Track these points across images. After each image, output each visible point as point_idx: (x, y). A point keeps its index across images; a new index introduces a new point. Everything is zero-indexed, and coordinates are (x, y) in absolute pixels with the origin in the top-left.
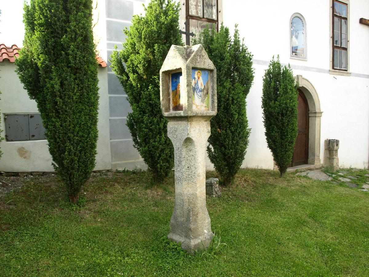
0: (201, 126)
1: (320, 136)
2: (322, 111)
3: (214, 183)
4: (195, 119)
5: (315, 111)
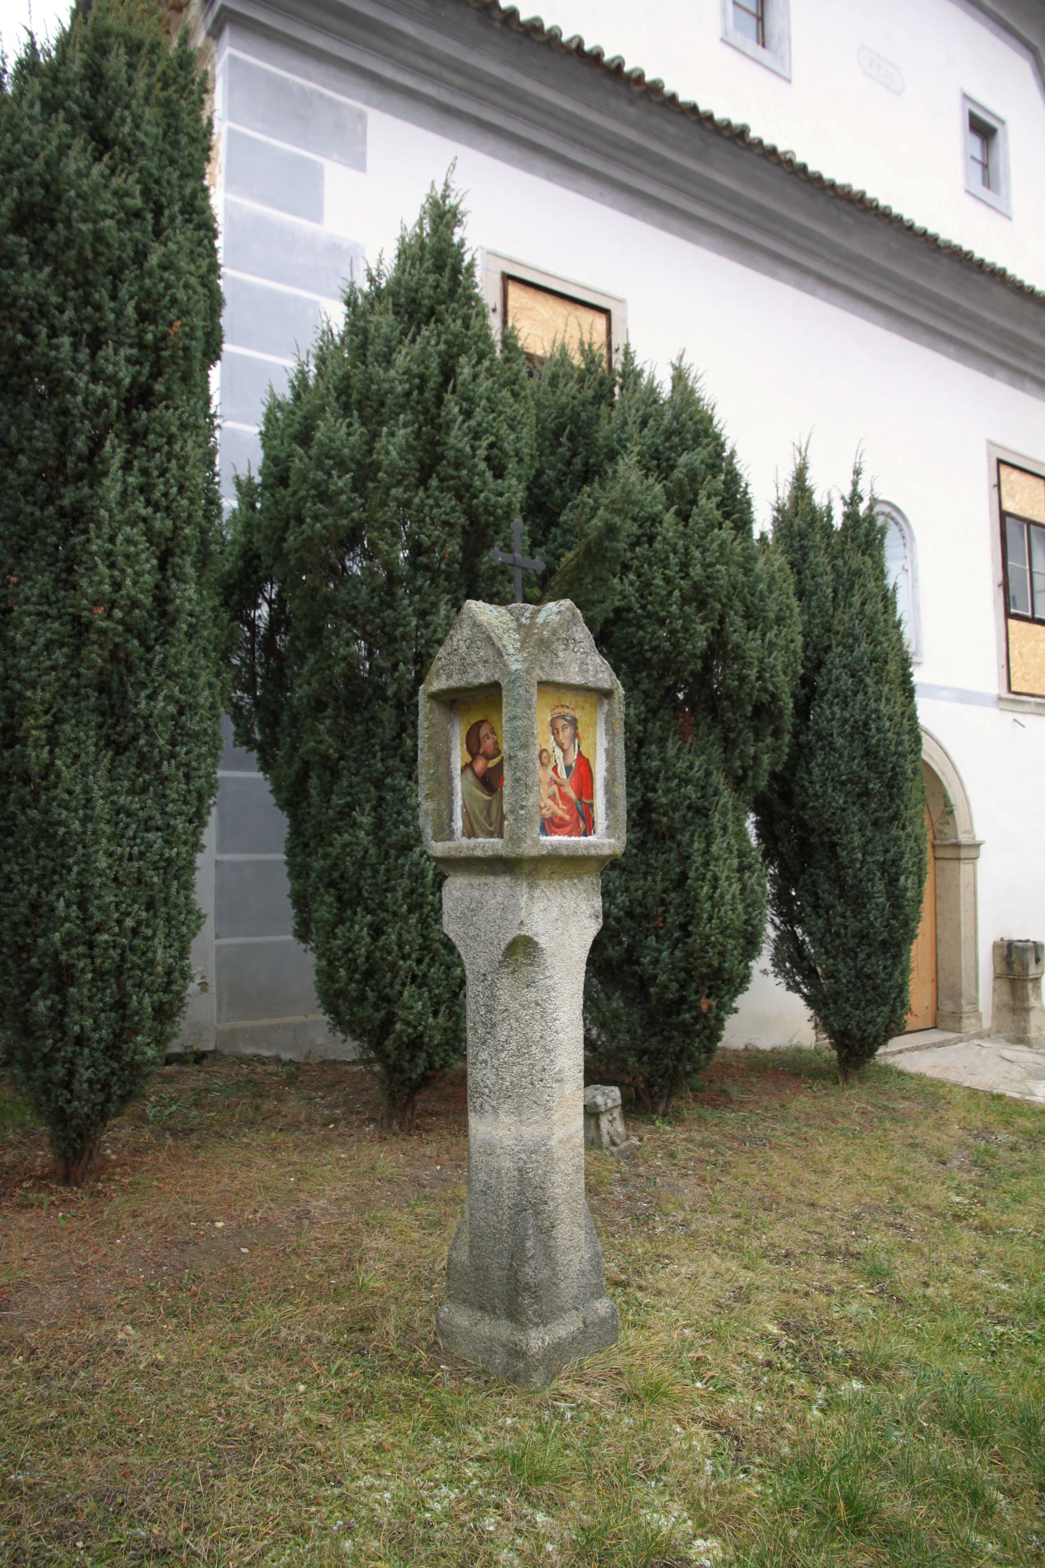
2: (979, 838)
5: (956, 837)
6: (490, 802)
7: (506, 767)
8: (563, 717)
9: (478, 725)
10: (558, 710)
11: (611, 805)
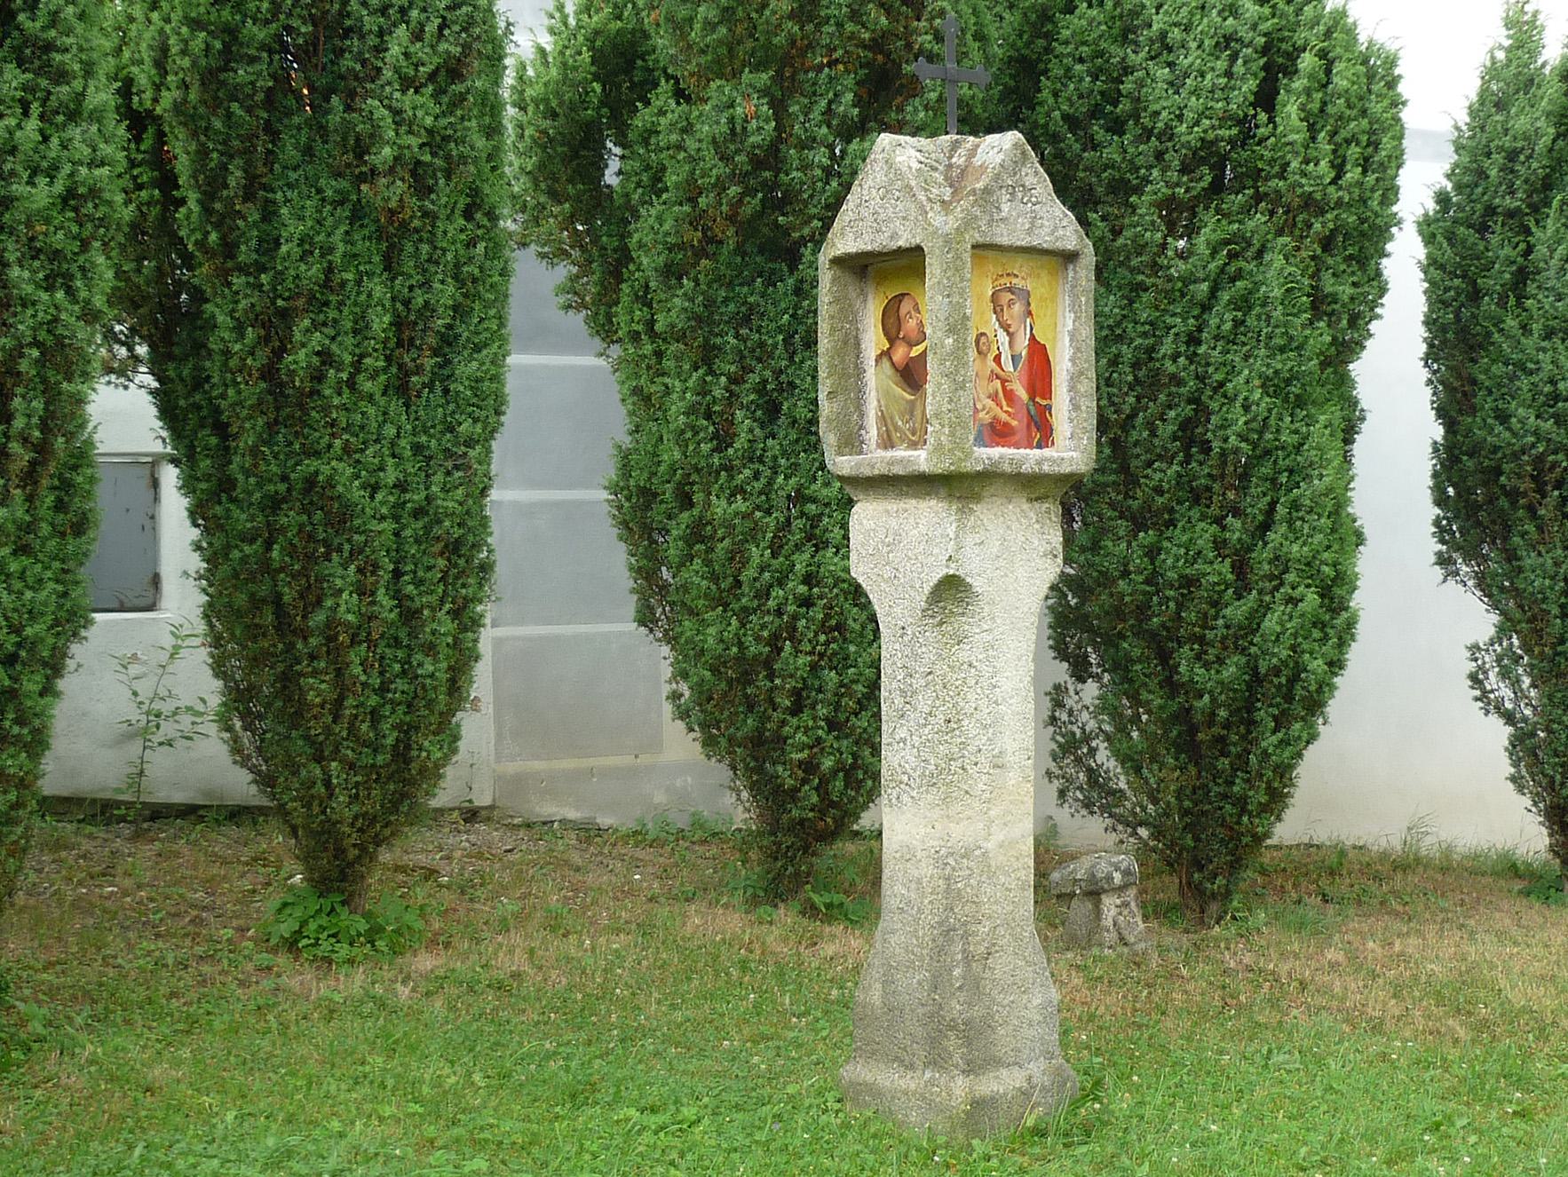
3: (1109, 878)
7: (929, 359)
8: (1010, 290)
10: (1002, 281)
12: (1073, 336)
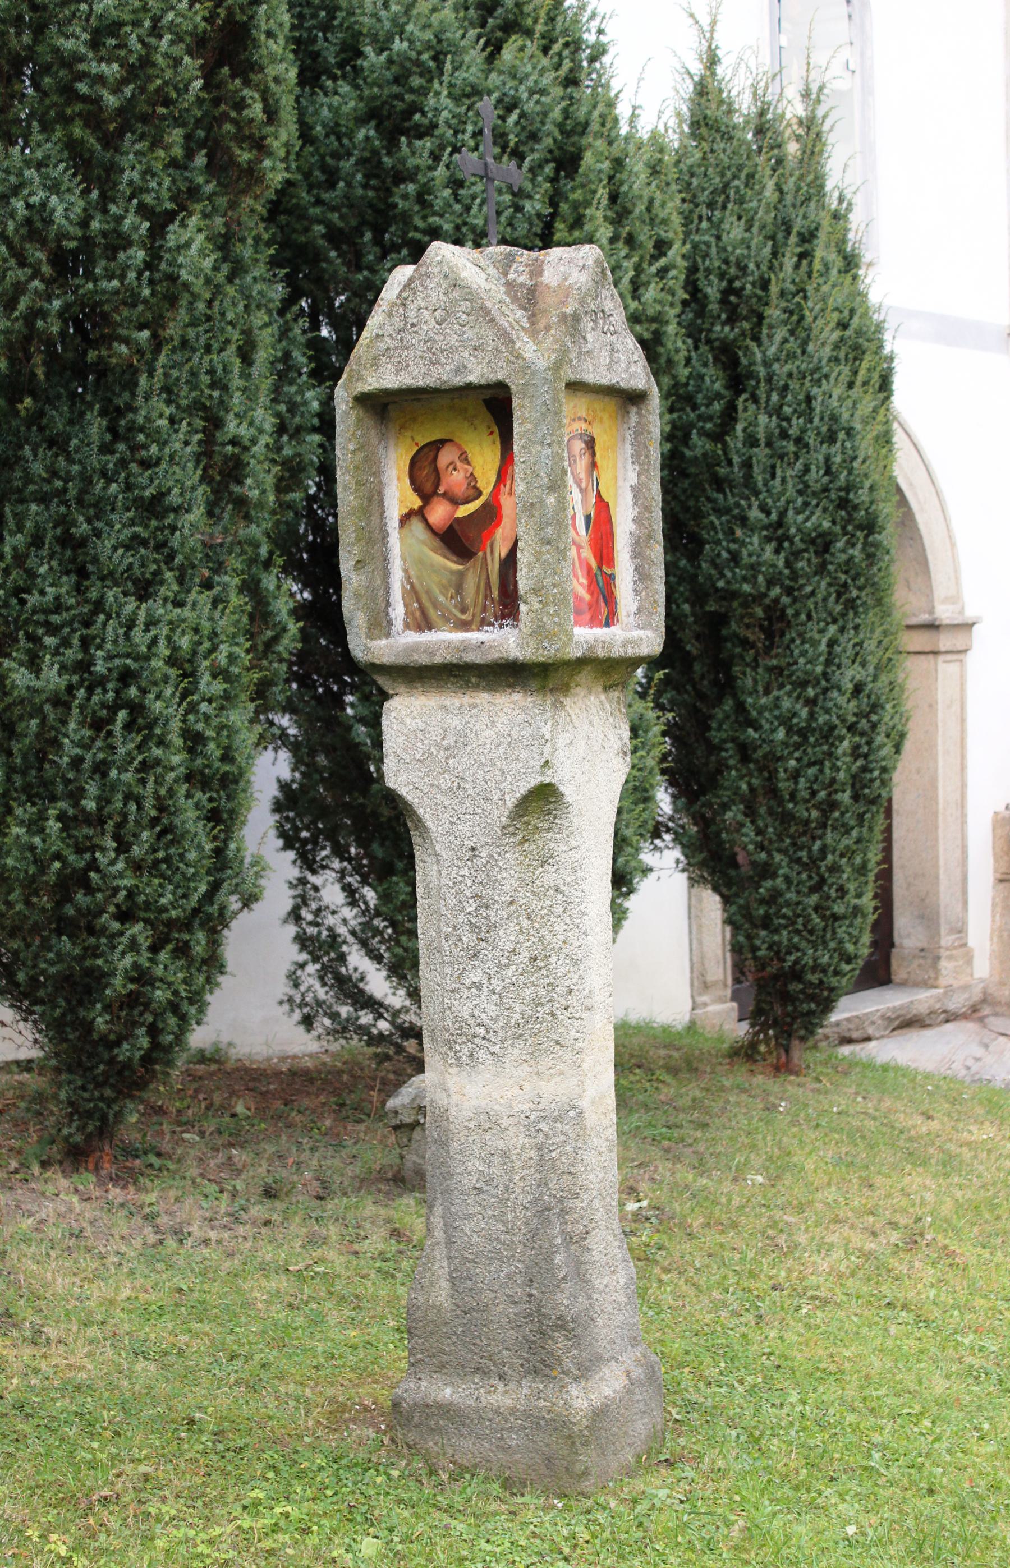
0: (596, 721)
1: (964, 786)
2: (970, 613)
4: (585, 676)
5: (931, 611)
6: (461, 575)
9: (438, 445)
11: (642, 575)
12: (637, 492)
